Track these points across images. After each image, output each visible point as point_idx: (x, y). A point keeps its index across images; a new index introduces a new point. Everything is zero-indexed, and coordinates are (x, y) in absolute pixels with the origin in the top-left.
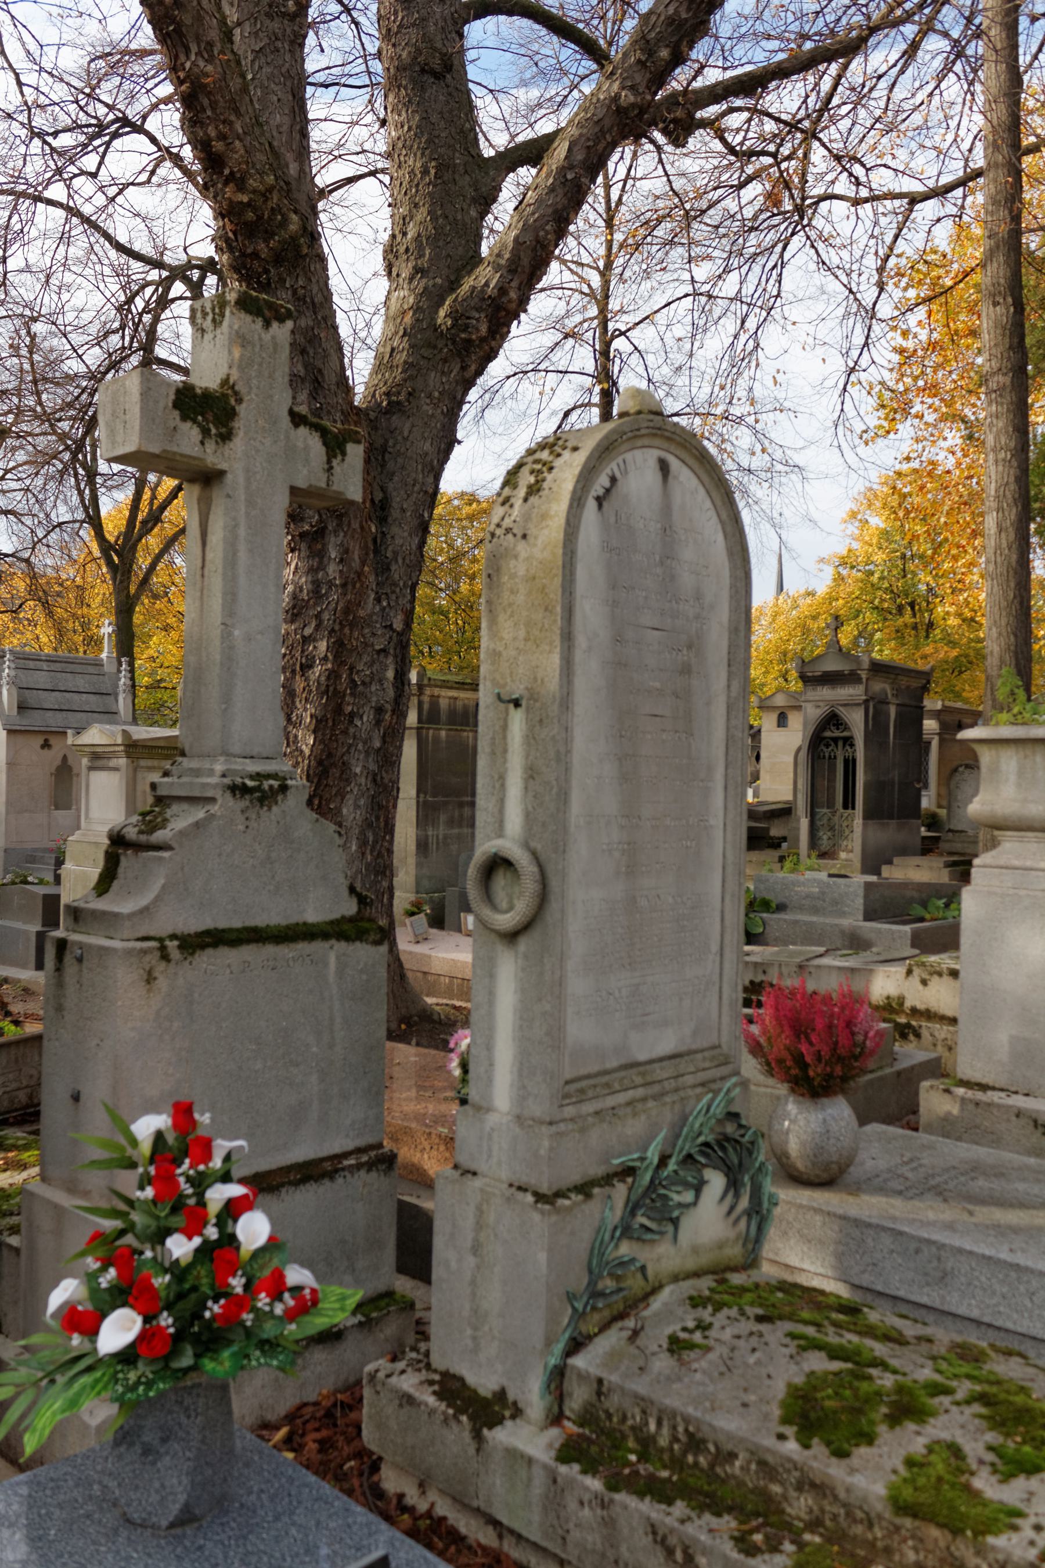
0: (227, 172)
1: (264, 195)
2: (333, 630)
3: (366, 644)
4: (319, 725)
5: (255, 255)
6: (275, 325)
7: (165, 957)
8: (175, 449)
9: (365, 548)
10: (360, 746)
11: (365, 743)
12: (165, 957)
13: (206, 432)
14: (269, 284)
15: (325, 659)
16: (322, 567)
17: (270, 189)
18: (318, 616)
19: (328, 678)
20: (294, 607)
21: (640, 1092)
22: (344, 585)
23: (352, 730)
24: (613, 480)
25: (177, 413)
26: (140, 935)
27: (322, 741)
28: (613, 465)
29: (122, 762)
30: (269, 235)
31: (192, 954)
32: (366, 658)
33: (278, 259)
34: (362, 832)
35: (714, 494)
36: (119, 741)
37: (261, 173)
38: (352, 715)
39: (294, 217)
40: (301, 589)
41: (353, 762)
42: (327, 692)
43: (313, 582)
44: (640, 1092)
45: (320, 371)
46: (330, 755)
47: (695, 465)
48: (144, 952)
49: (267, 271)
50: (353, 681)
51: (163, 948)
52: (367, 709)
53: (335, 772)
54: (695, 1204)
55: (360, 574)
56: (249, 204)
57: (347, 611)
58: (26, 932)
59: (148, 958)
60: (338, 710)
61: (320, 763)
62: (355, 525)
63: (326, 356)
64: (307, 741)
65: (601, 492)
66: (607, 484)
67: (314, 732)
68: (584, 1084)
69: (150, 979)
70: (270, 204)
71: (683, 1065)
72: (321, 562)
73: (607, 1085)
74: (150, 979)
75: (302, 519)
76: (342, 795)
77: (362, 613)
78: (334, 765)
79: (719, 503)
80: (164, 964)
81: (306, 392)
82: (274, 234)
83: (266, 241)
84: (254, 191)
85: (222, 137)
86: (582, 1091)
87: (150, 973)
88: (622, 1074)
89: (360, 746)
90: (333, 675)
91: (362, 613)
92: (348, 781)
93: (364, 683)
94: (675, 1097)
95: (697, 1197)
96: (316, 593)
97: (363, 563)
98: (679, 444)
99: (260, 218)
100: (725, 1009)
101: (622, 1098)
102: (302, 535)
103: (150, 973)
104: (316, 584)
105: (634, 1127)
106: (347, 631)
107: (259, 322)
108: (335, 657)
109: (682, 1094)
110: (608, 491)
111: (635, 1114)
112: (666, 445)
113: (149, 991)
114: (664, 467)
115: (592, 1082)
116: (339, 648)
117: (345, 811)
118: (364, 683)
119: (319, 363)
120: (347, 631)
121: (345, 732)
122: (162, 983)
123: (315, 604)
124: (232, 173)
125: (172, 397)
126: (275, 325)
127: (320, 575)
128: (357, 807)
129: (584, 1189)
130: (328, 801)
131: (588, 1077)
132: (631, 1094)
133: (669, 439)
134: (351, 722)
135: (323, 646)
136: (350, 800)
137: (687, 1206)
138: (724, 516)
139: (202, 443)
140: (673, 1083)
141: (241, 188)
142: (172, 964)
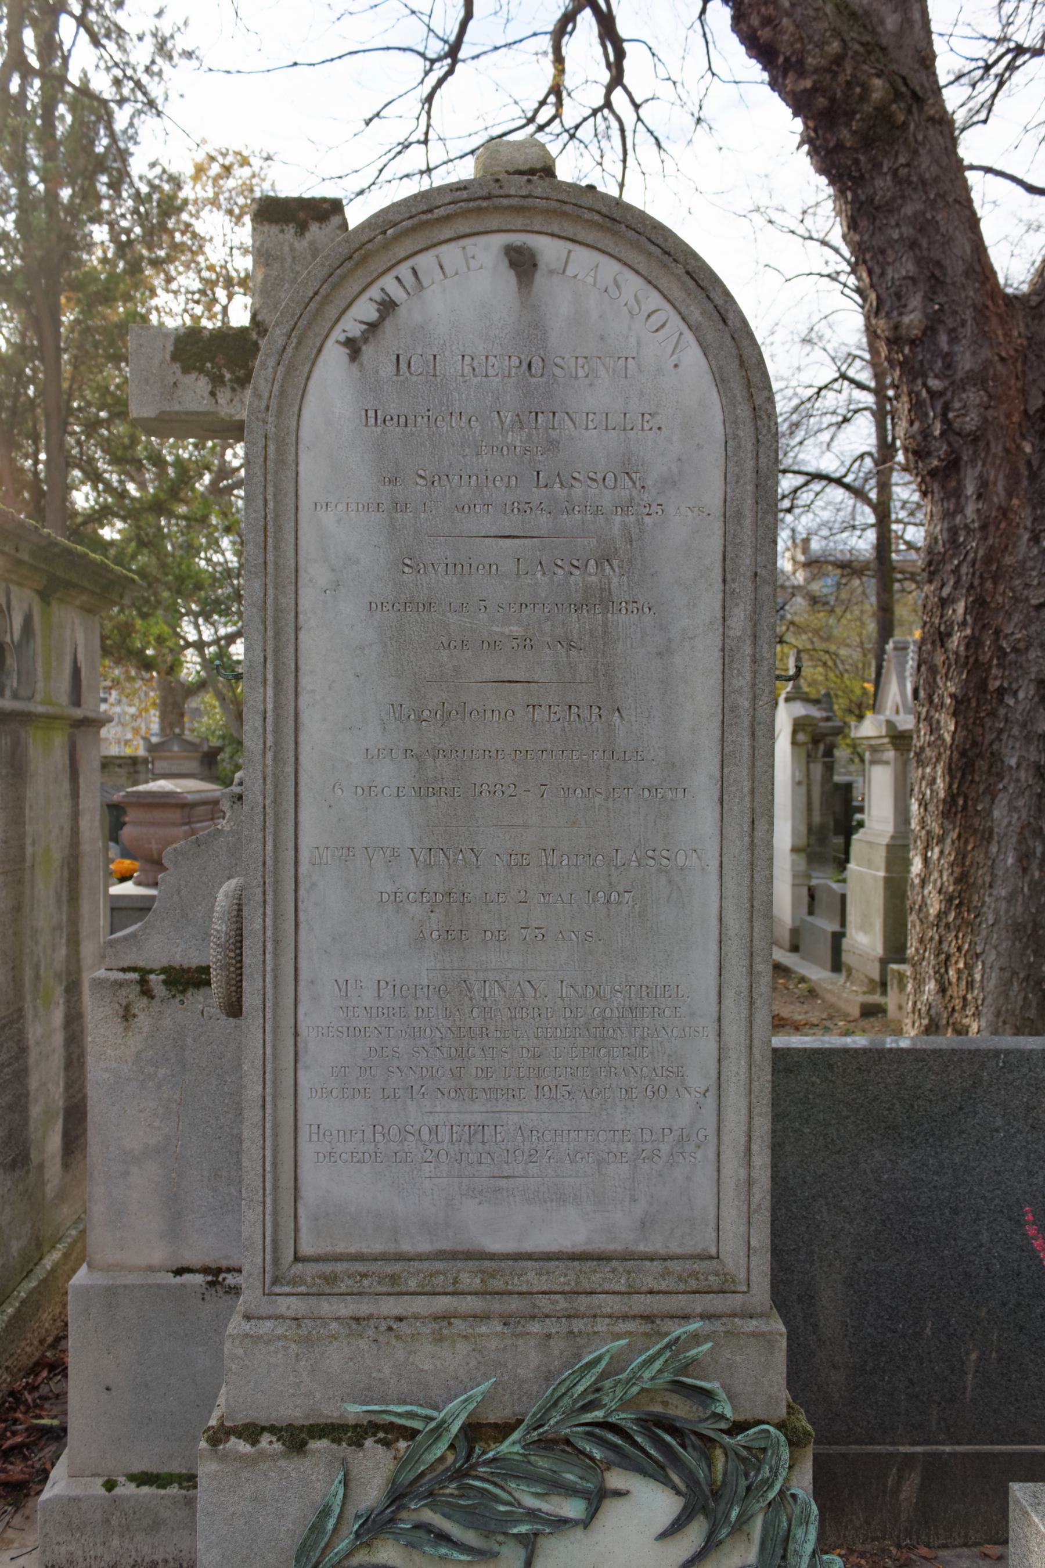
0: (781, 60)
1: (829, 70)
2: (972, 586)
3: (1016, 600)
4: (960, 706)
5: (840, 146)
6: (314, 227)
7: (146, 992)
8: (177, 408)
9: (1014, 477)
10: (1016, 731)
11: (1024, 725)
12: (146, 992)
13: (217, 381)
14: (862, 176)
15: (964, 624)
16: (960, 510)
17: (838, 60)
18: (956, 571)
19: (967, 647)
20: (930, 564)
21: (471, 1304)
22: (984, 527)
23: (1002, 711)
24: (388, 306)
25: (177, 367)
26: (126, 965)
27: (965, 727)
28: (388, 282)
29: (890, 754)
30: (850, 114)
31: (183, 992)
32: (1017, 617)
33: (867, 141)
34: (1022, 840)
35: (663, 282)
36: (884, 733)
37: (821, 45)
38: (1001, 691)
39: (877, 82)
40: (936, 540)
41: (1004, 751)
42: (966, 664)
43: (949, 529)
44: (471, 1304)
45: (938, 264)
46: (975, 744)
47: (607, 241)
48: (120, 984)
49: (856, 161)
50: (1001, 648)
51: (143, 982)
52: (1024, 683)
53: (982, 764)
54: (586, 1523)
55: (1005, 511)
56: (815, 89)
57: (988, 560)
58: (825, 931)
59: (123, 992)
60: (982, 686)
61: (963, 754)
62: (997, 449)
63: (948, 241)
64: (949, 726)
65: (355, 330)
66: (373, 315)
67: (955, 714)
68: (340, 1267)
69: (127, 1015)
70: (841, 79)
71: (598, 1277)
72: (958, 504)
73: (394, 1278)
74: (127, 1015)
75: (929, 454)
76: (992, 794)
77: (1008, 560)
78: (980, 755)
79: (677, 294)
80: (145, 1000)
81: (919, 297)
82: (854, 113)
83: (848, 125)
84: (816, 71)
85: (767, 21)
86: (331, 1279)
87: (127, 1008)
88: (439, 1265)
89: (1016, 731)
90: (973, 643)
91: (1008, 560)
92: (1000, 776)
93: (1015, 650)
94: (563, 1326)
95: (593, 1514)
96: (953, 541)
97: (1010, 495)
98: (547, 212)
99: (833, 100)
100: (729, 1194)
101: (420, 1305)
102: (933, 473)
103: (127, 1008)
104: (953, 531)
105: (437, 1361)
106: (989, 585)
107: (291, 229)
108: (975, 621)
109: (578, 1325)
110: (373, 327)
111: (439, 1339)
112: (519, 222)
113: (126, 1029)
114: (522, 263)
115: (360, 1267)
116: (980, 607)
117: (996, 814)
118: (1015, 650)
119: (936, 254)
120: (989, 585)
121: (993, 714)
122: (143, 1021)
123: (953, 556)
124: (787, 60)
125: (170, 348)
126: (314, 227)
127: (958, 518)
128: (1012, 808)
129: (296, 1438)
130: (976, 801)
131: (359, 1258)
132: (443, 1303)
133: (520, 210)
134: (1001, 701)
135: (960, 607)
136: (1003, 800)
137: (562, 1523)
138: (696, 314)
139: (213, 394)
140: (562, 1303)
141: (802, 74)
142: (156, 1002)
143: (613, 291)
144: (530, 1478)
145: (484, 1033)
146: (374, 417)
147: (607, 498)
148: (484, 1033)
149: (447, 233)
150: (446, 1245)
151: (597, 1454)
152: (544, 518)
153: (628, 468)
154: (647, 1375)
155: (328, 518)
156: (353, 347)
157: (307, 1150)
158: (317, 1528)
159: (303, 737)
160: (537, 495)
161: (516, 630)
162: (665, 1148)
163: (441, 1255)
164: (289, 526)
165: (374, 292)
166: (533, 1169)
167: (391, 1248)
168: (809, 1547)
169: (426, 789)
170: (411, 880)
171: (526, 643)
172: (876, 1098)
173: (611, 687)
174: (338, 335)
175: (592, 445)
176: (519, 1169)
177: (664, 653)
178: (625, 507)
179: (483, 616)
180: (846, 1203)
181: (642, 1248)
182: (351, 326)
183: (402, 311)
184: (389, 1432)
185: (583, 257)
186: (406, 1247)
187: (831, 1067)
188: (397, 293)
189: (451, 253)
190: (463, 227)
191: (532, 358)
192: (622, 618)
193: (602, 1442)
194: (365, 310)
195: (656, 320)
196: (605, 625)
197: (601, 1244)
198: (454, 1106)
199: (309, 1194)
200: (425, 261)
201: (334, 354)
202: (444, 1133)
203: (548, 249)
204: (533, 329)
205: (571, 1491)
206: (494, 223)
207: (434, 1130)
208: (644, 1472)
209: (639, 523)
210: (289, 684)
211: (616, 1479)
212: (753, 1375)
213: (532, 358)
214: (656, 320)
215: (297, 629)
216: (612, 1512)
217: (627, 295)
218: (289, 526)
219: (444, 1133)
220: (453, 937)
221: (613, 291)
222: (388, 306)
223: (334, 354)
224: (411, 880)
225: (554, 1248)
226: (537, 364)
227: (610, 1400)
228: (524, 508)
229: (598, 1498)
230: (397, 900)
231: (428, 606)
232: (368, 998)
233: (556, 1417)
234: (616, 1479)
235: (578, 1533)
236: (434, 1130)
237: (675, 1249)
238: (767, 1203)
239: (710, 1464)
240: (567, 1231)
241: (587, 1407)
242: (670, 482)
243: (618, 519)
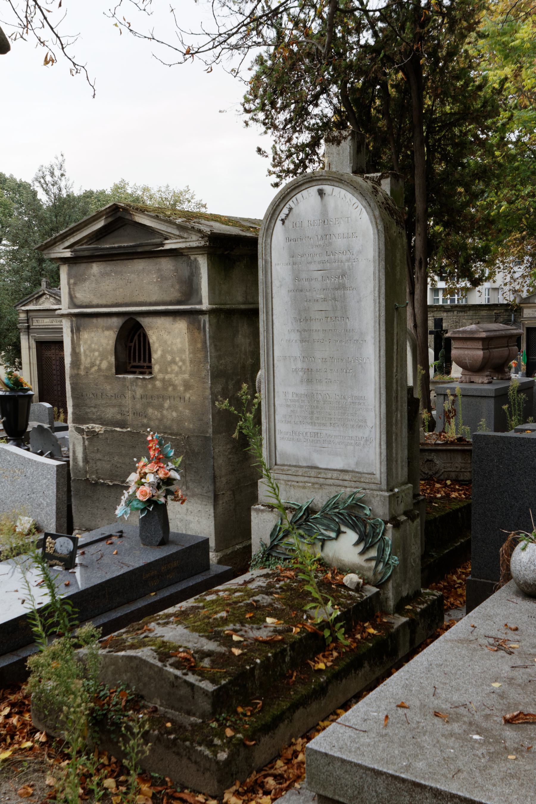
24: (290, 209)
28: (290, 203)
47: (341, 185)
54: (336, 538)
110: (287, 215)
143: (344, 199)
144: (323, 525)
145: (317, 407)
146: (288, 239)
147: (344, 258)
148: (317, 407)
149: (303, 188)
150: (310, 465)
151: (337, 520)
152: (328, 265)
153: (349, 249)
154: (350, 501)
155: (278, 267)
156: (283, 221)
157: (278, 436)
158: (275, 529)
159: (274, 327)
160: (326, 258)
161: (323, 296)
162: (362, 442)
163: (308, 467)
164: (269, 271)
165: (287, 206)
166: (330, 446)
167: (297, 464)
168: (388, 553)
169: (302, 341)
170: (299, 365)
171: (325, 300)
172: (527, 457)
173: (346, 311)
174: (279, 218)
175: (339, 243)
176: (326, 445)
177: (359, 301)
178: (348, 260)
179: (314, 293)
180: (515, 495)
181: (357, 470)
182: (282, 216)
183: (294, 210)
184: (292, 509)
185: (337, 190)
186: (301, 464)
187: (510, 443)
188: (292, 205)
189: (304, 193)
190: (307, 186)
191: (325, 220)
192: (348, 292)
193: (339, 518)
194: (285, 211)
195: (355, 206)
196: (344, 294)
197: (346, 468)
198: (311, 427)
199: (278, 448)
200: (299, 196)
201: (279, 223)
202: (309, 434)
203: (327, 188)
204: (324, 212)
205: (332, 530)
206: (314, 183)
207: (306, 433)
208: (350, 528)
209: (352, 264)
210: (270, 313)
211: (343, 529)
212: (378, 507)
213: (325, 220)
214: (355, 206)
215: (272, 298)
216: (342, 537)
217: (348, 200)
218: (269, 271)
219: (309, 434)
220: (309, 381)
221: (344, 199)
222: (290, 209)
223: (279, 223)
224: (299, 365)
225: (335, 468)
226: (326, 221)
227: (341, 507)
228: (323, 262)
229: (339, 533)
230: (296, 370)
231: (302, 291)
232: (290, 397)
233: (328, 509)
234: (343, 529)
235: (334, 541)
236: (306, 433)
237: (365, 471)
238: (385, 460)
239: (365, 528)
240: (338, 463)
241: (335, 508)
242: (360, 252)
243: (347, 264)
